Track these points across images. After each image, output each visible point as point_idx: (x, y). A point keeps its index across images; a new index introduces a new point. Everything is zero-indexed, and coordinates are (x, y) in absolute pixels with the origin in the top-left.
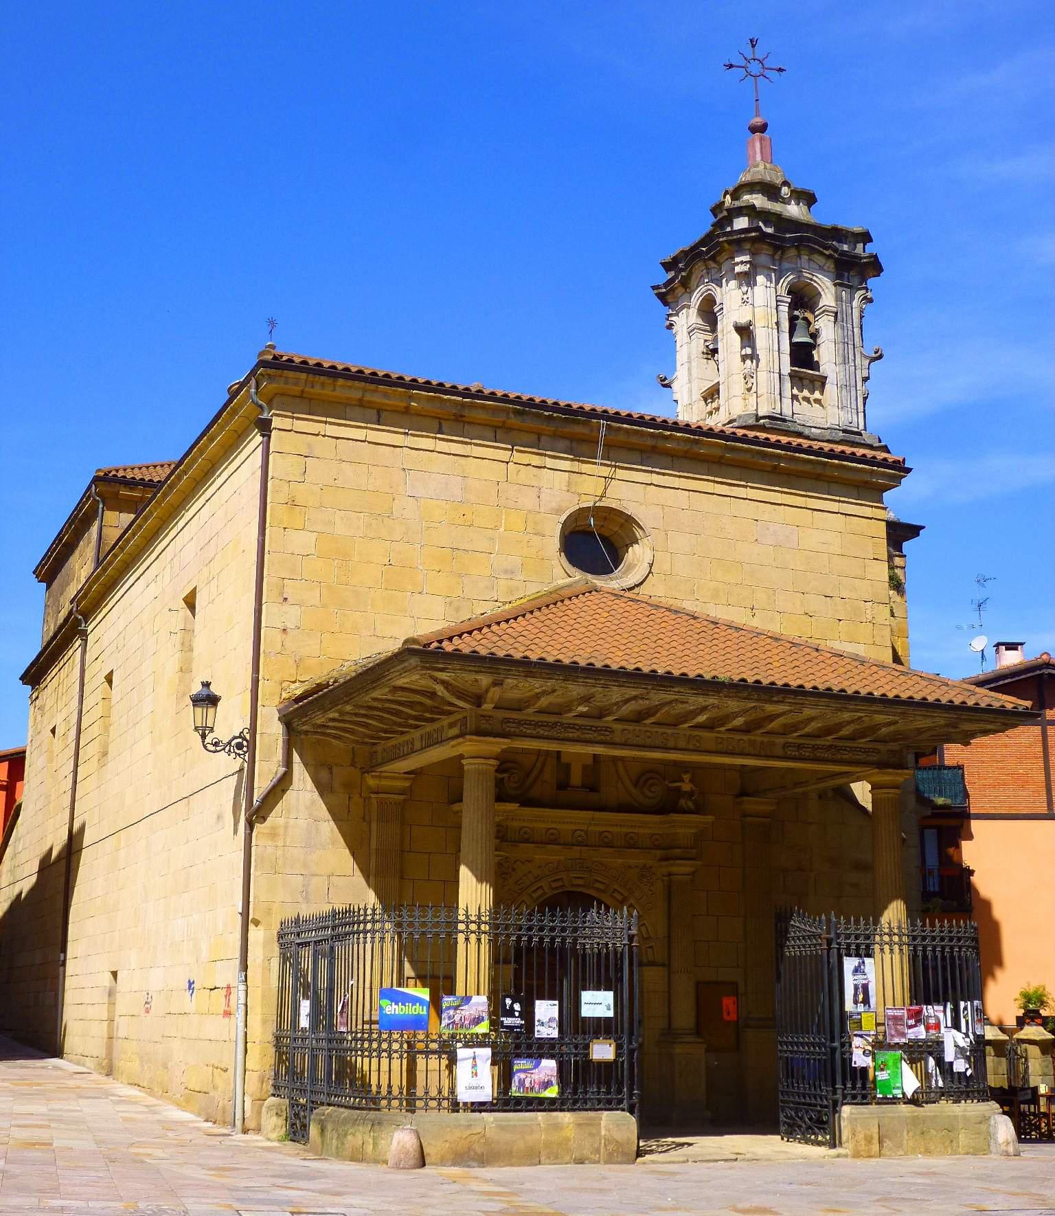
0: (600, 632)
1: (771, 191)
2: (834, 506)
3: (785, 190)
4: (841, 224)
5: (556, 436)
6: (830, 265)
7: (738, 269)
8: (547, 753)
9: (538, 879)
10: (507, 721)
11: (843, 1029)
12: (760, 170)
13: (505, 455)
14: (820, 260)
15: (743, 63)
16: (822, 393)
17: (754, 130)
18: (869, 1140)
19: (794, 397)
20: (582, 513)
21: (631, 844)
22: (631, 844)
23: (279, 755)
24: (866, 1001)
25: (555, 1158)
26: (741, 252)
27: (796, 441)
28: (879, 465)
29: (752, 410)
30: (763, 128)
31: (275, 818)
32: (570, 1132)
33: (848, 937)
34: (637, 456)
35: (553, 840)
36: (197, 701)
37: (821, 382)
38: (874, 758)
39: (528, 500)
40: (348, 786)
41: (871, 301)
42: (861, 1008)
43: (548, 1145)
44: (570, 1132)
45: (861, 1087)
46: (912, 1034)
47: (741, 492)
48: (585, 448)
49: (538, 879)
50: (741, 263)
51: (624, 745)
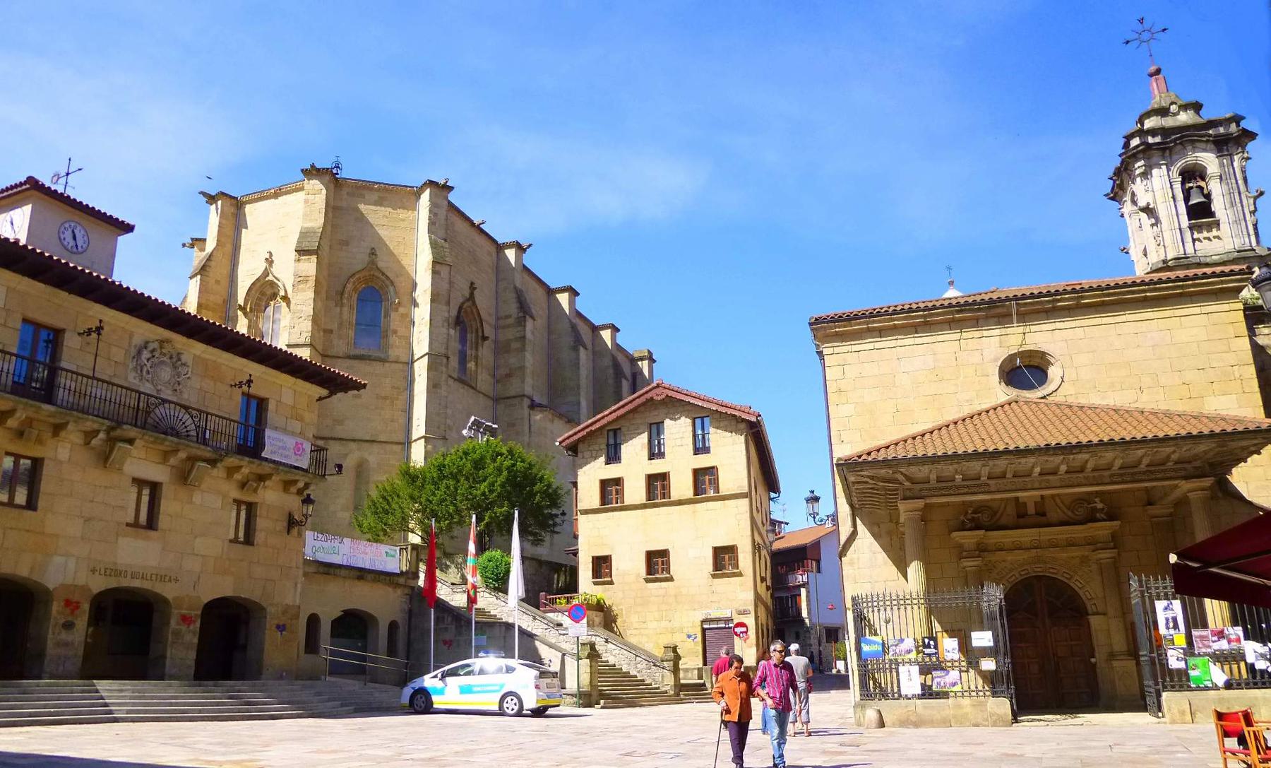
0: (1030, 425)
1: (1163, 112)
2: (1197, 310)
3: (1173, 108)
4: (1213, 118)
5: (987, 317)
6: (1211, 146)
7: (1137, 172)
8: (1007, 499)
9: (1011, 570)
10: (921, 490)
11: (1160, 646)
12: (1157, 101)
13: (957, 336)
14: (1203, 145)
15: (1136, 36)
16: (1219, 229)
17: (1151, 75)
18: (1183, 713)
19: (1194, 240)
20: (1011, 358)
21: (1071, 544)
22: (1071, 544)
23: (849, 522)
24: (1176, 627)
25: (961, 724)
26: (1138, 160)
27: (1200, 271)
28: (1174, 281)
29: (1163, 258)
30: (1158, 72)
31: (851, 553)
32: (968, 710)
33: (1157, 588)
34: (1044, 315)
35: (1018, 547)
36: (808, 500)
37: (1217, 224)
38: (1183, 473)
39: (976, 358)
40: (889, 533)
41: (1248, 159)
42: (1172, 631)
43: (954, 717)
44: (968, 710)
45: (1180, 680)
46: (1216, 646)
47: (1123, 318)
48: (1006, 319)
49: (1011, 570)
50: (1139, 166)
51: (999, 491)
